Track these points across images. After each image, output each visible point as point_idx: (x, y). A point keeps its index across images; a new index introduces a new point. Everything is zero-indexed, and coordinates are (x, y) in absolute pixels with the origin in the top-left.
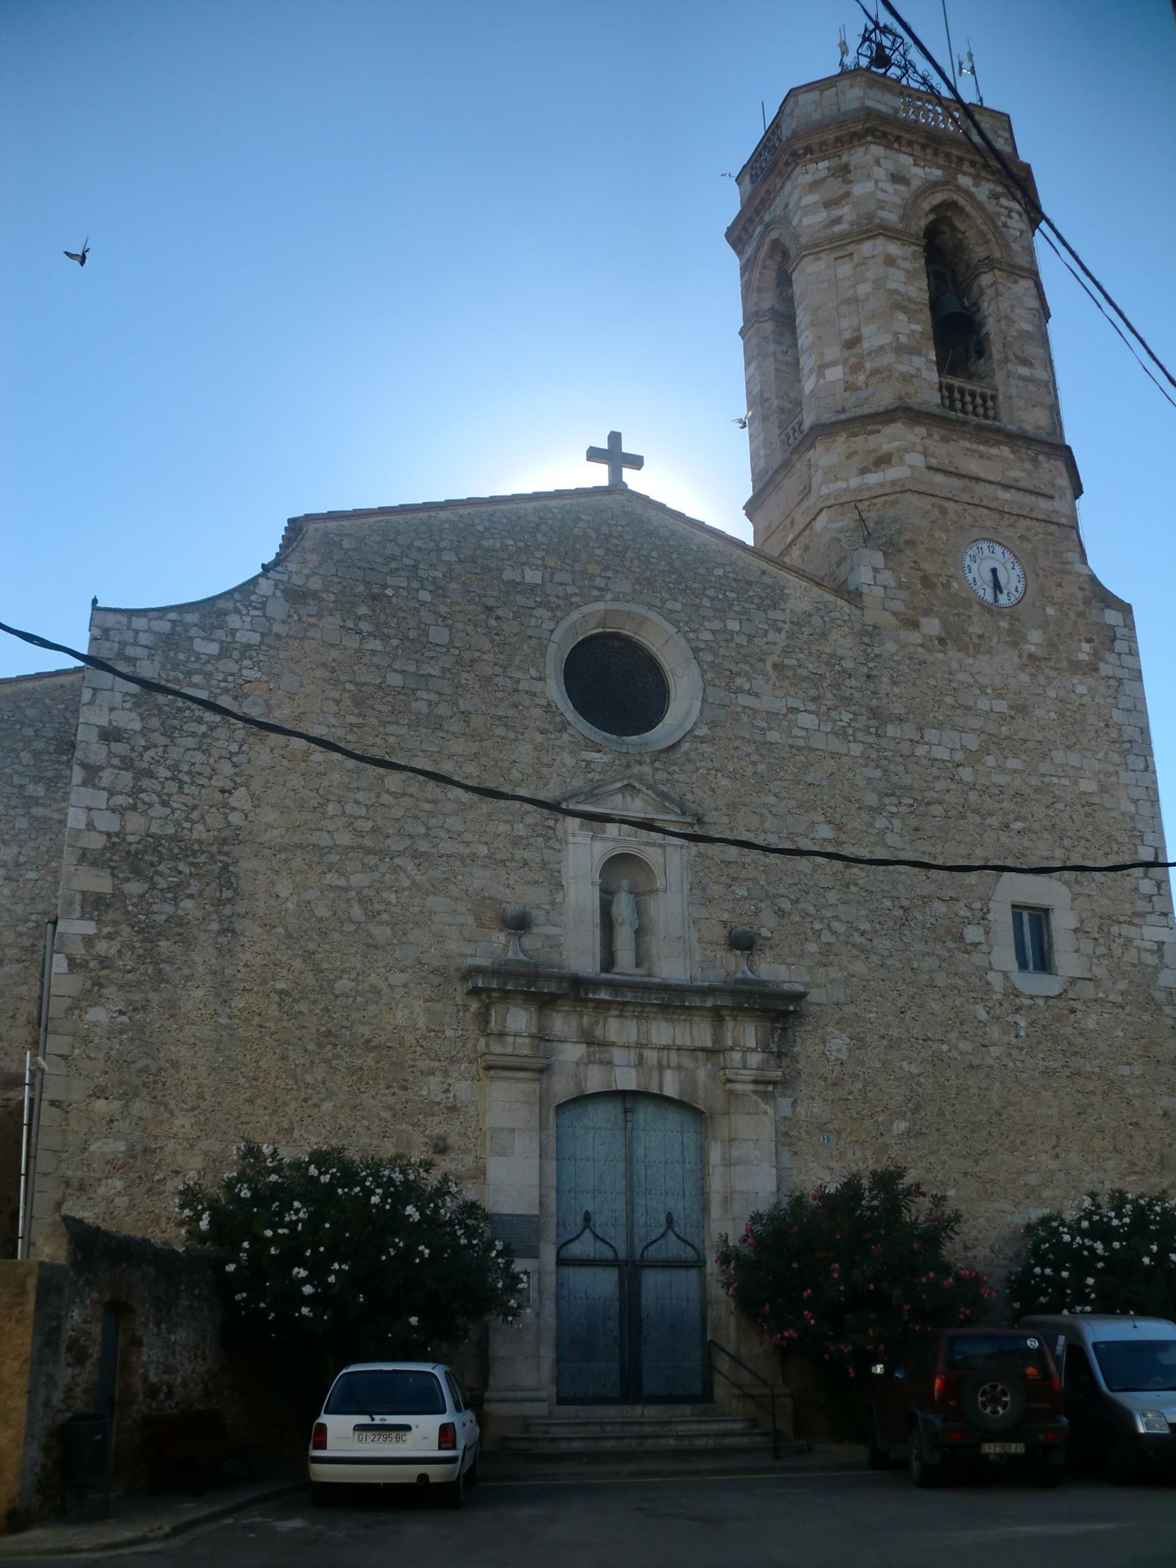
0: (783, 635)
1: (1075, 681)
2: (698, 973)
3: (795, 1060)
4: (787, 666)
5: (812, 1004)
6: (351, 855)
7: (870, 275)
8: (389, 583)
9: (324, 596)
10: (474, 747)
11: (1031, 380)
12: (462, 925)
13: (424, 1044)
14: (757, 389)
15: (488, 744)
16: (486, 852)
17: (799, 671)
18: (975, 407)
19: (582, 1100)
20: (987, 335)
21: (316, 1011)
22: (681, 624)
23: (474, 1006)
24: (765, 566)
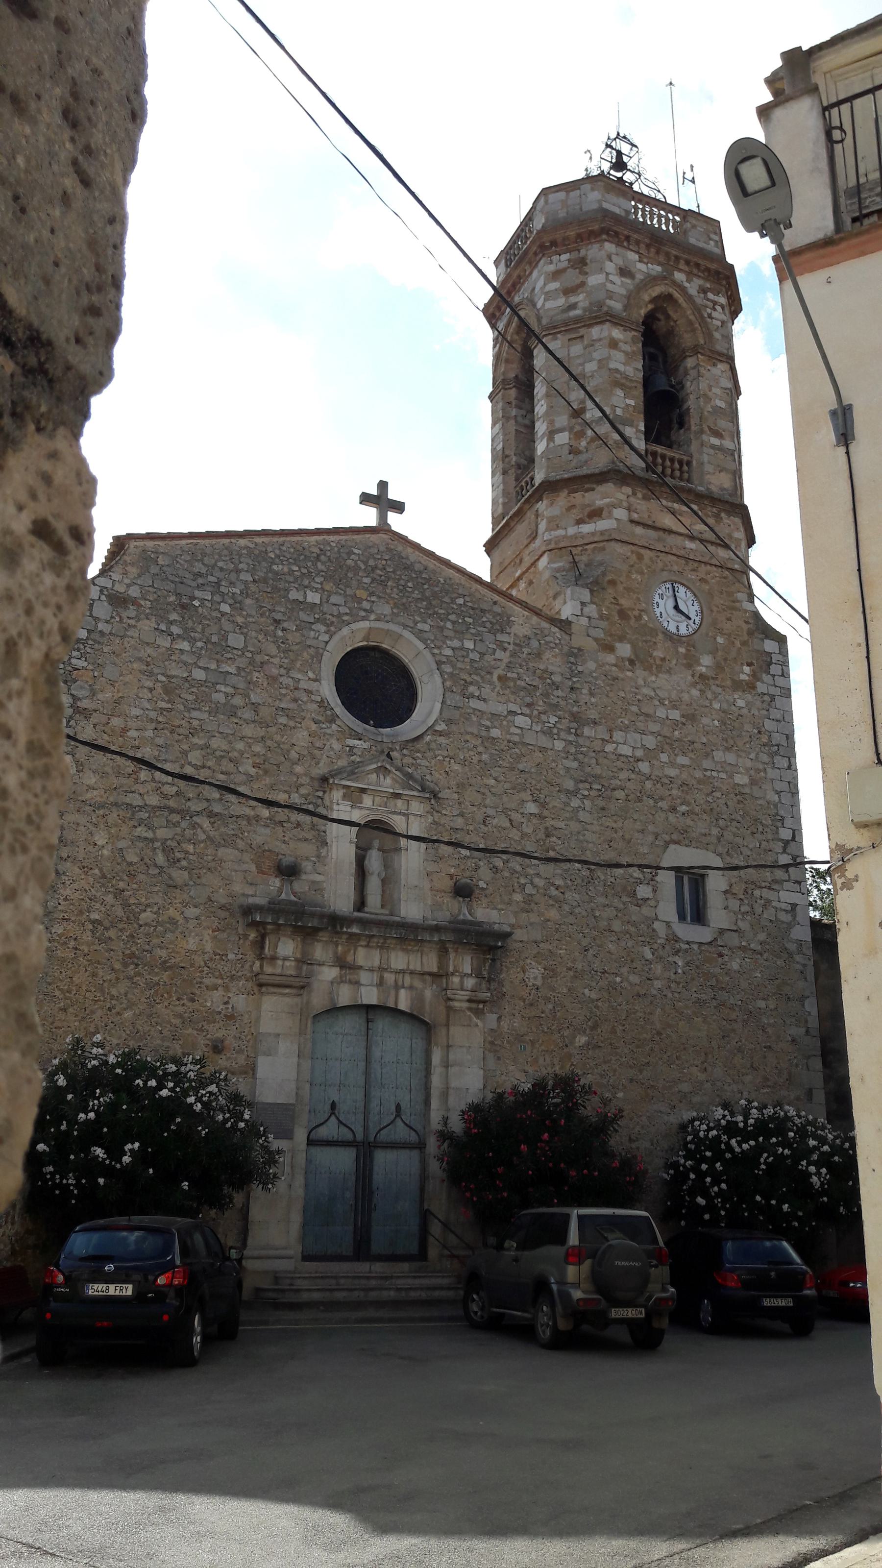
0: (508, 653)
1: (736, 696)
2: (429, 914)
3: (501, 984)
4: (509, 678)
5: (516, 941)
6: (157, 814)
7: (596, 355)
8: (196, 596)
9: (142, 603)
10: (261, 732)
11: (720, 449)
12: (246, 871)
13: (210, 965)
14: (500, 447)
15: (273, 730)
16: (268, 815)
17: (519, 682)
18: (673, 471)
19: (334, 1011)
20: (688, 409)
21: (124, 937)
22: (429, 642)
23: (253, 935)
24: (496, 598)
